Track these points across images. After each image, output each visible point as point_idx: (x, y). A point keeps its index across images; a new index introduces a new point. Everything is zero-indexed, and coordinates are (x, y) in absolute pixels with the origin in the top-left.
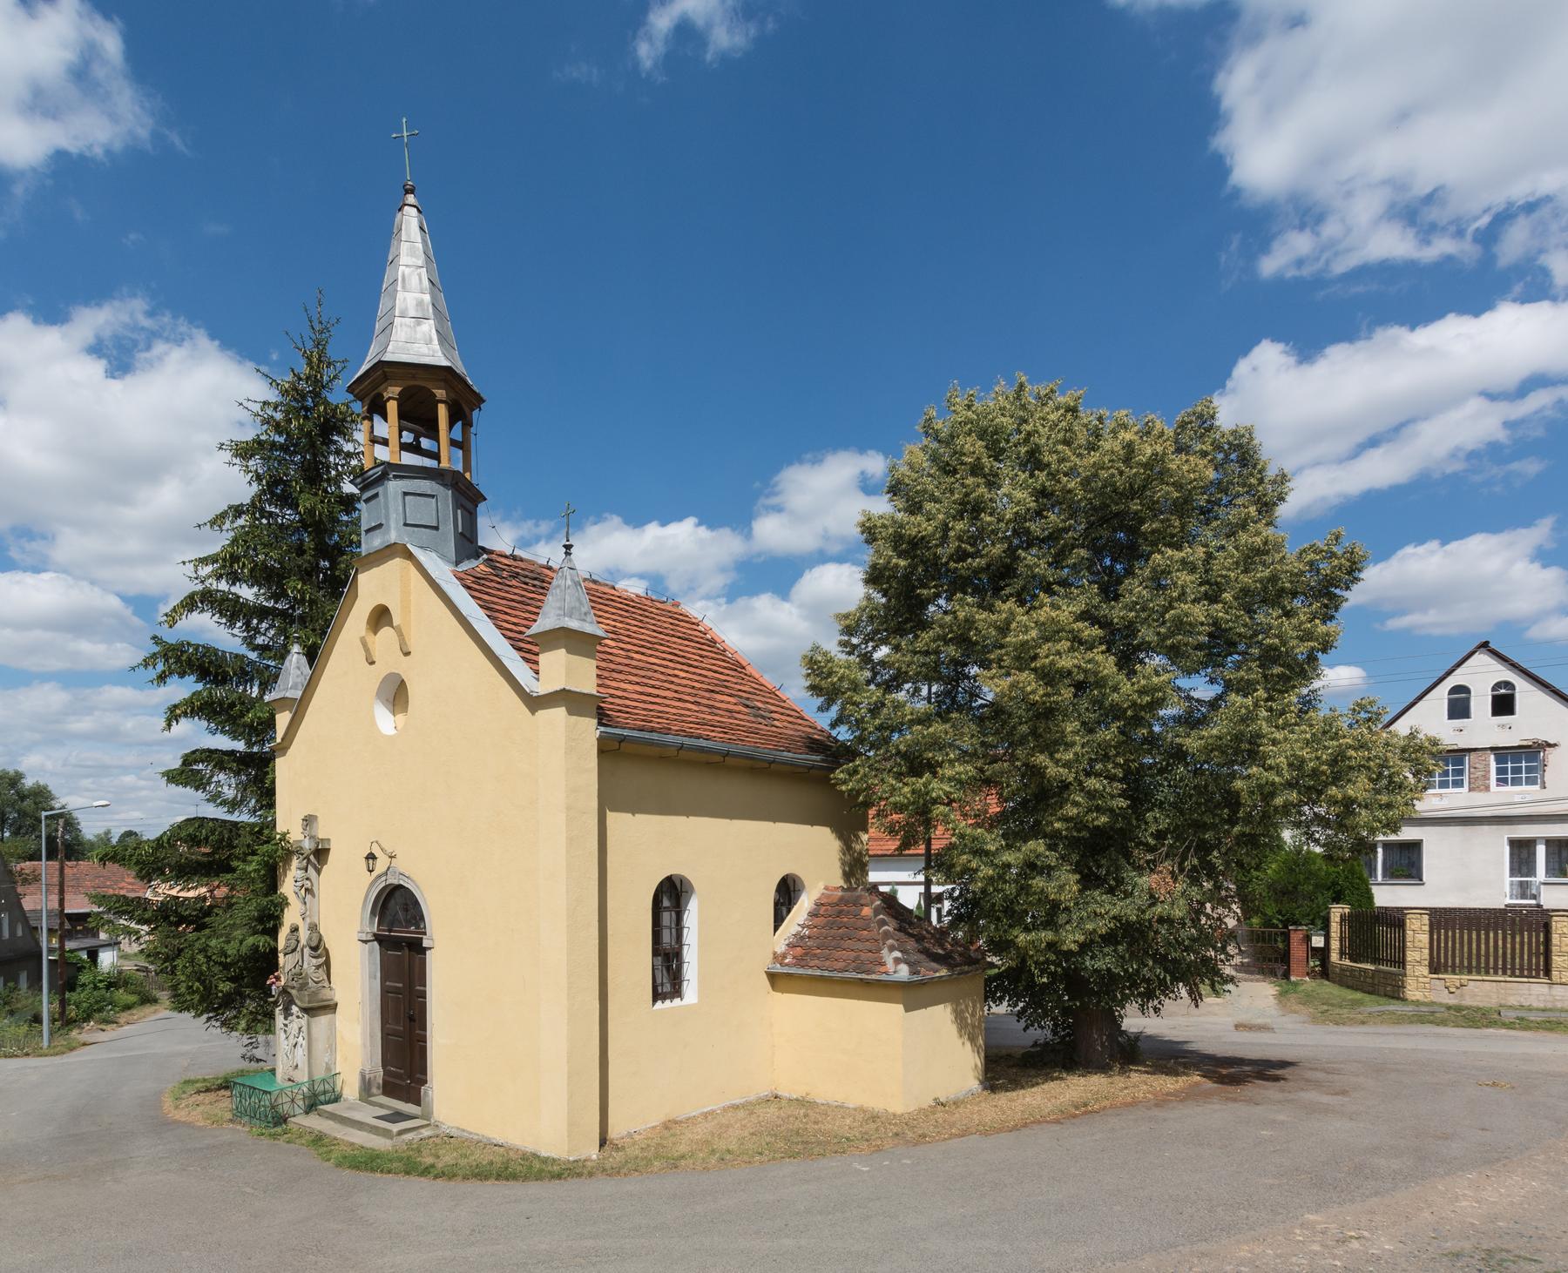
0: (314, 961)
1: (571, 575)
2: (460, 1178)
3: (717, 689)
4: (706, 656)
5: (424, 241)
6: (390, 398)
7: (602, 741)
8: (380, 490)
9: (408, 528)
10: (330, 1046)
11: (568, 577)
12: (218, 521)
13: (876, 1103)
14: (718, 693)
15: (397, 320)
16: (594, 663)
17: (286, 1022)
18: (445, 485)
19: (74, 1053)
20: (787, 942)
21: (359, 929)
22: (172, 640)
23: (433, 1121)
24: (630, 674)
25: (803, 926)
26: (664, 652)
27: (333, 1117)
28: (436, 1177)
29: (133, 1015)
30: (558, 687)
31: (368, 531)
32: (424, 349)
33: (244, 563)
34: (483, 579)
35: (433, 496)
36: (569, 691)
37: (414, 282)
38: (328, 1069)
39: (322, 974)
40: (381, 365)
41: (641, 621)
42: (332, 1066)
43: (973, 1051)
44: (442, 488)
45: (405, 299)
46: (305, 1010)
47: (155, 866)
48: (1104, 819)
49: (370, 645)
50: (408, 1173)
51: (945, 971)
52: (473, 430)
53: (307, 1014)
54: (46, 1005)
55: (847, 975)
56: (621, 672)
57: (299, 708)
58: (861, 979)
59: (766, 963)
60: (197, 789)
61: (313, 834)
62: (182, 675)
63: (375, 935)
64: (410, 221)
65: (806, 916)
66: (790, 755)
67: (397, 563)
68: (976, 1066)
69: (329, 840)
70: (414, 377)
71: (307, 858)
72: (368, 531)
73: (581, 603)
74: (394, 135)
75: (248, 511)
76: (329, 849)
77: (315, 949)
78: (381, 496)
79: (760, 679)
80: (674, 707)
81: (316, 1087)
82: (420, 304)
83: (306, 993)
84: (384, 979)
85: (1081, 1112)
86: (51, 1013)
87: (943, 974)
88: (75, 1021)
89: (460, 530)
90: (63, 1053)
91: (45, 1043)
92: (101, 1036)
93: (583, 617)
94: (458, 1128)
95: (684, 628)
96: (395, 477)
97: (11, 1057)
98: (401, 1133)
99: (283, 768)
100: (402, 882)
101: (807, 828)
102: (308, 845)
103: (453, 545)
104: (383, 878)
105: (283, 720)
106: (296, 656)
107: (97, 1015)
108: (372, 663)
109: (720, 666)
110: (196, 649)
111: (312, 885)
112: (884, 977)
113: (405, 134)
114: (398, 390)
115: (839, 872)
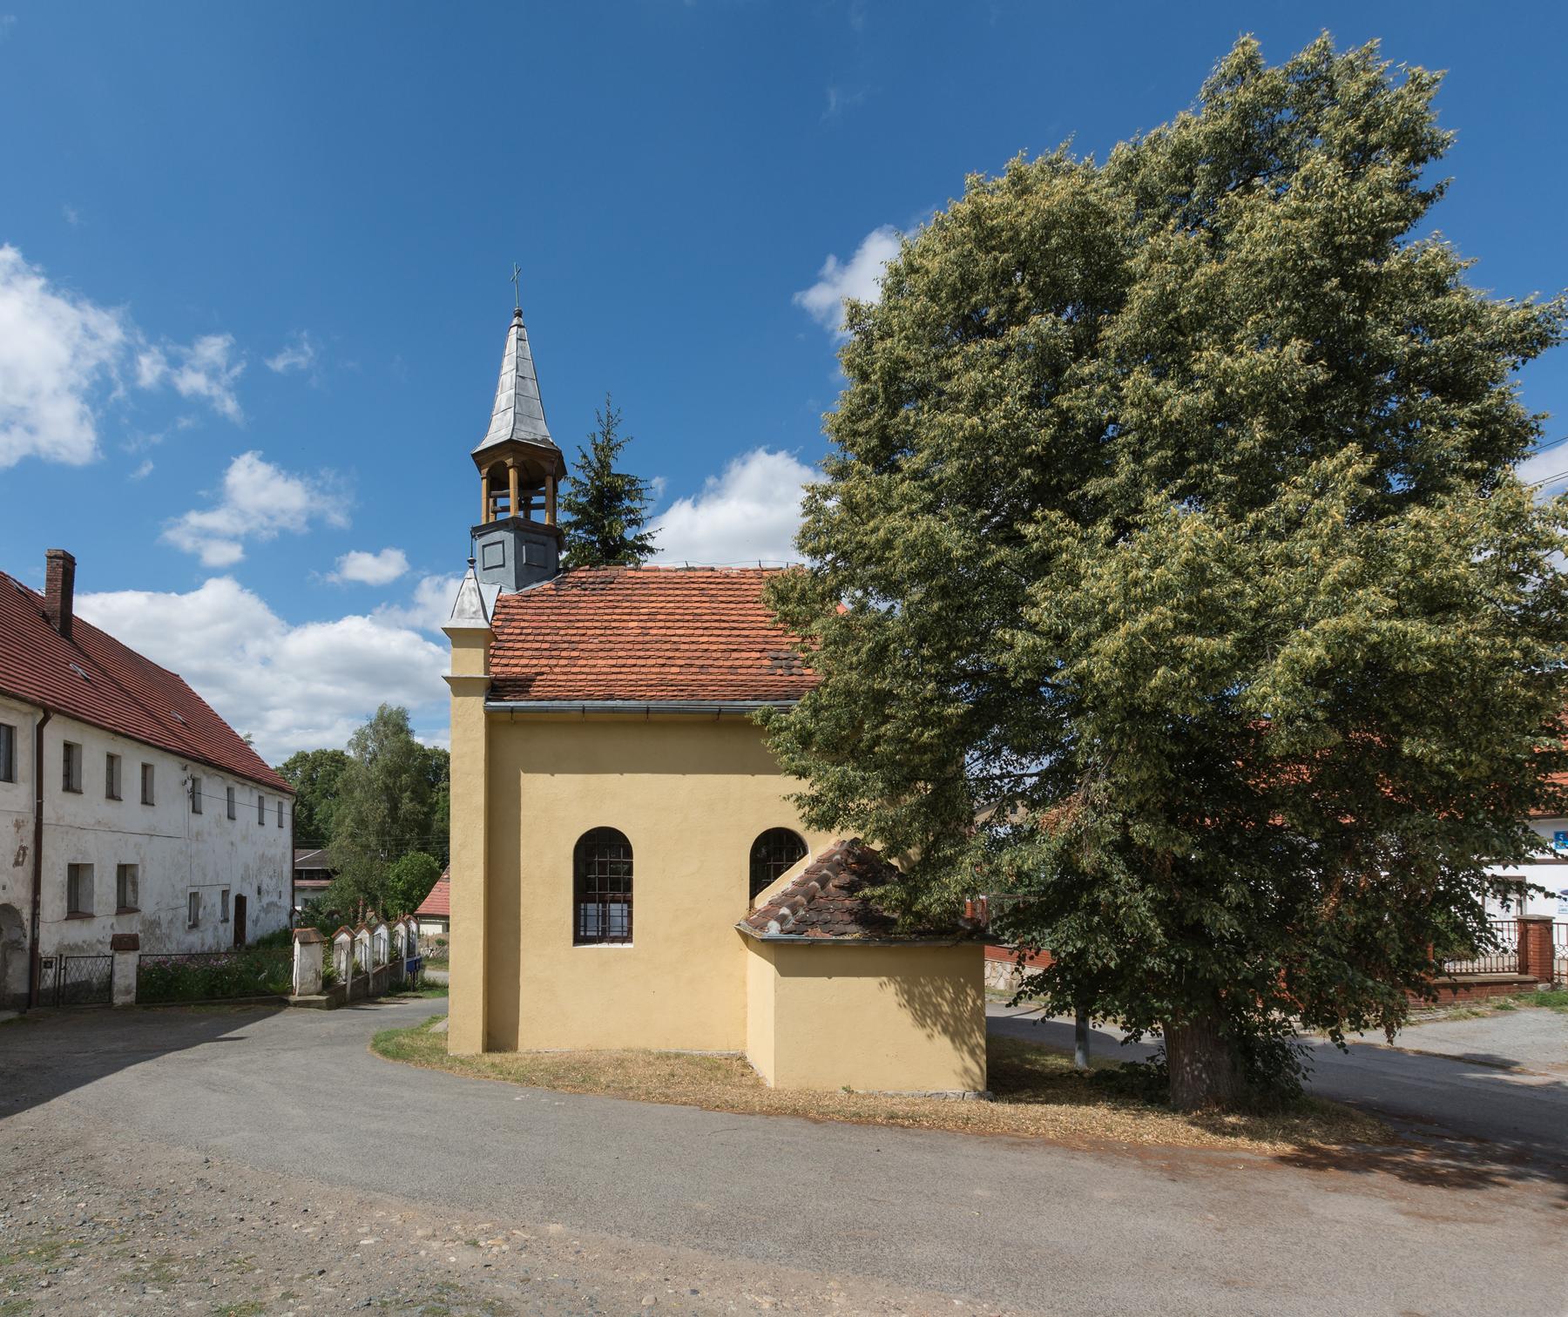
64: (513, 333)
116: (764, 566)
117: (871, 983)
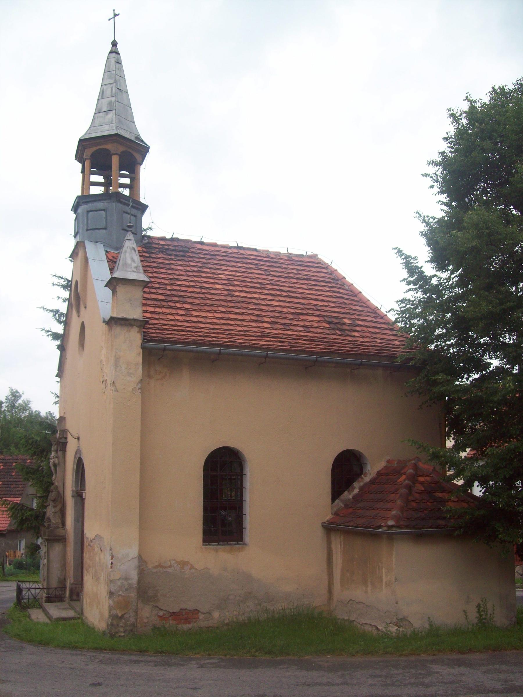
3: (305, 312)
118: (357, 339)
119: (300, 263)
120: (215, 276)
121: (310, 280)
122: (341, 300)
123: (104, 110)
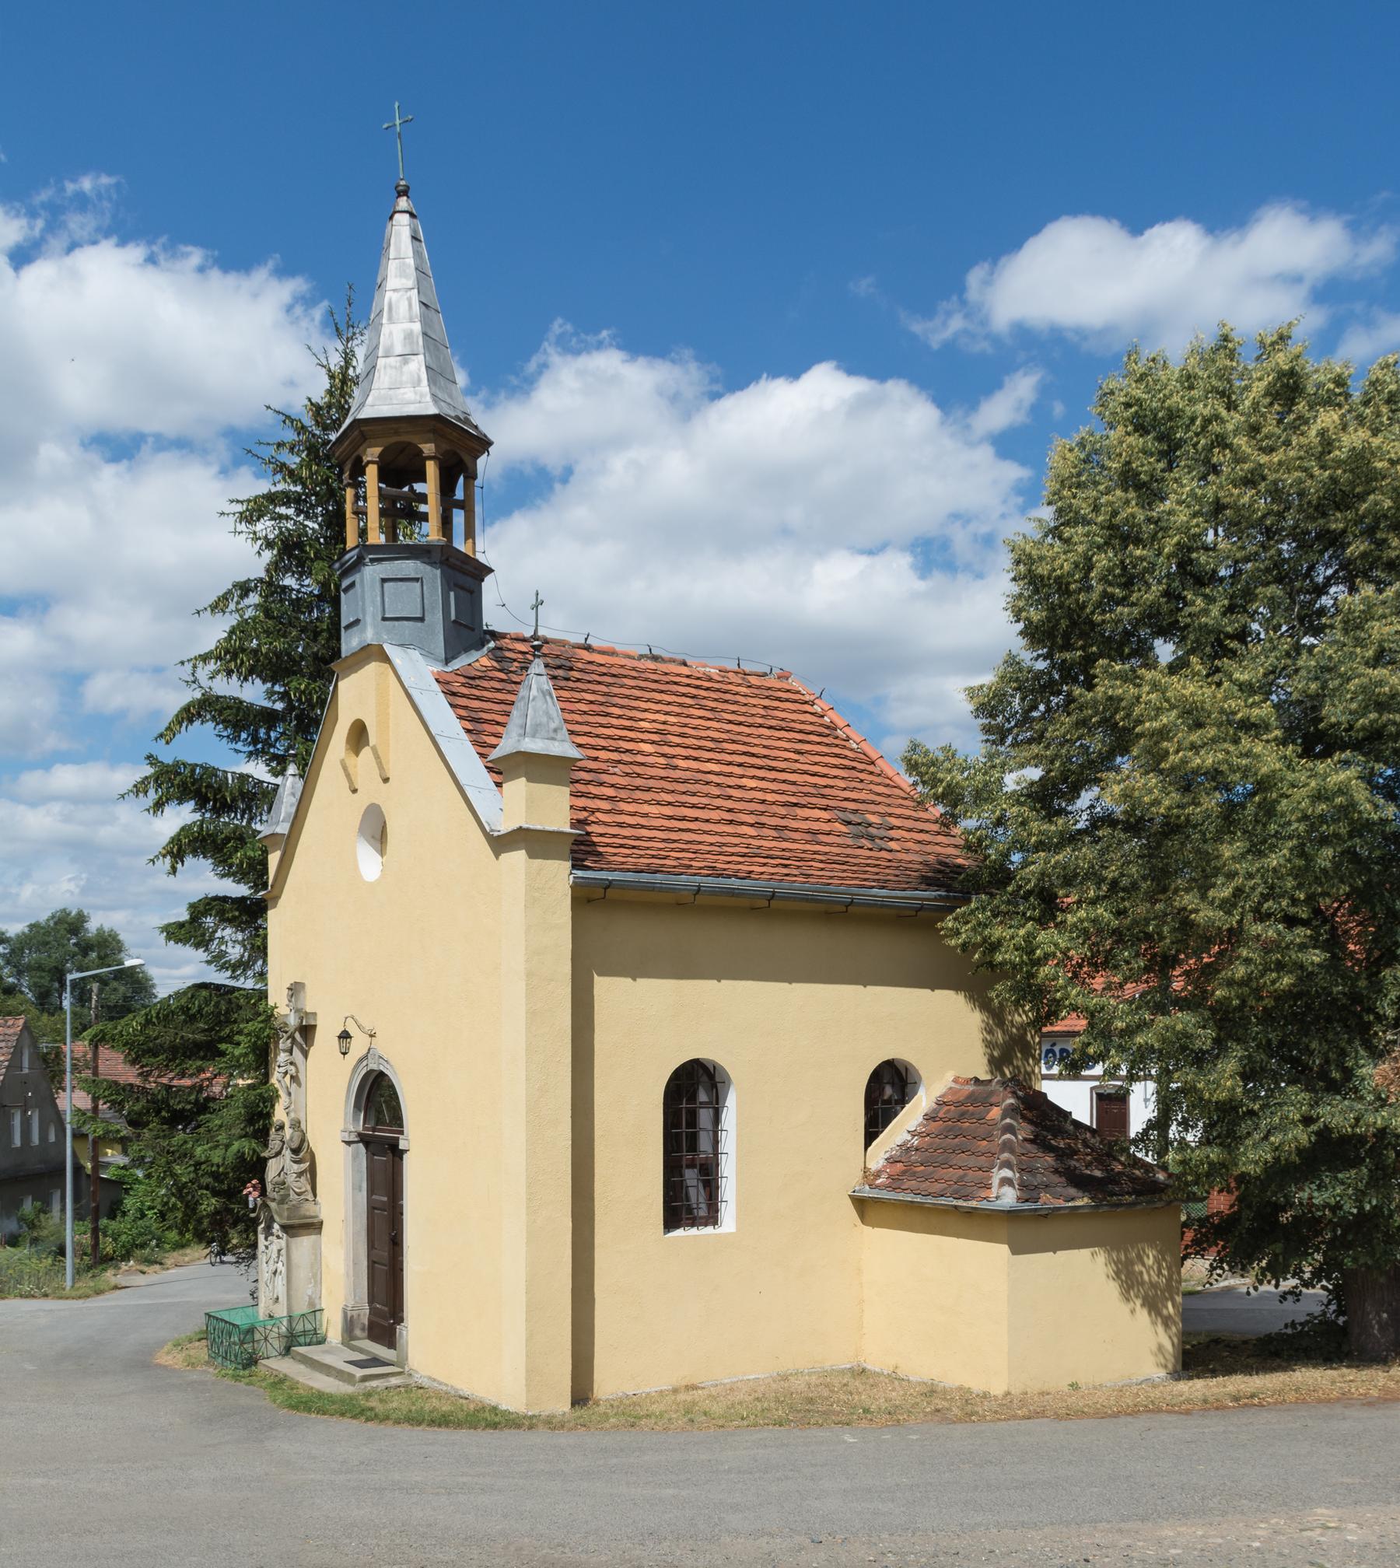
0: (295, 1166)
1: (537, 683)
2: (391, 1422)
3: (803, 801)
4: (807, 752)
5: (417, 254)
6: (369, 462)
7: (575, 887)
8: (356, 577)
9: (387, 623)
10: (314, 1276)
11: (534, 686)
12: (219, 606)
13: (977, 1385)
14: (804, 806)
15: (381, 362)
16: (566, 790)
17: (267, 1243)
18: (432, 564)
19: (101, 1297)
20: (887, 1155)
21: (342, 1128)
22: (168, 760)
23: (407, 1369)
24: (663, 790)
25: (913, 1134)
26: (734, 753)
27: (306, 1361)
28: (368, 1420)
29: (186, 1255)
30: (515, 826)
31: (348, 627)
32: (409, 394)
33: (242, 662)
34: (480, 678)
35: (416, 580)
36: (528, 830)
37: (402, 309)
38: (311, 1303)
39: (304, 1184)
40: (357, 422)
41: (712, 709)
42: (317, 1301)
43: (1154, 1323)
44: (428, 568)
45: (391, 333)
46: (285, 1228)
47: (145, 1047)
48: (1287, 981)
49: (351, 770)
50: (343, 1415)
51: (1086, 1200)
52: (478, 482)
53: (286, 1233)
54: (72, 1233)
55: (942, 1201)
56: (649, 789)
57: (289, 843)
58: (956, 1207)
59: (853, 1181)
60: (197, 946)
61: (299, 1007)
62: (181, 801)
63: (359, 1135)
64: (401, 228)
65: (921, 1119)
66: (884, 892)
67: (373, 668)
68: (1160, 1348)
69: (315, 1014)
70: (397, 433)
71: (292, 1037)
72: (348, 627)
73: (550, 718)
74: (385, 126)
75: (256, 587)
76: (315, 1026)
77: (296, 1151)
78: (357, 585)
79: (896, 778)
80: (717, 833)
81: (294, 1325)
82: (409, 336)
83: (286, 1206)
84: (371, 1191)
85: (1211, 1407)
86: (77, 1245)
87: (1079, 1203)
88: (112, 1259)
89: (453, 617)
90: (87, 1296)
91: (69, 1283)
92: (140, 1280)
93: (552, 735)
94: (430, 1378)
95: (786, 713)
96: (372, 561)
97: (27, 1297)
98: (365, 1379)
99: (275, 920)
100: (382, 1068)
101: (925, 993)
102: (293, 1021)
103: (442, 638)
104: (365, 1063)
105: (274, 859)
106: (291, 779)
107: (138, 1252)
108: (355, 791)
109: (826, 765)
110: (193, 771)
111: (297, 1071)
112: (984, 1205)
113: (398, 122)
114: (377, 450)
115: (984, 1062)
116: (747, 667)
117: (1085, 1253)
118: (900, 856)
119: (767, 693)
120: (634, 724)
121: (791, 730)
122: (855, 774)
123: (399, 350)
